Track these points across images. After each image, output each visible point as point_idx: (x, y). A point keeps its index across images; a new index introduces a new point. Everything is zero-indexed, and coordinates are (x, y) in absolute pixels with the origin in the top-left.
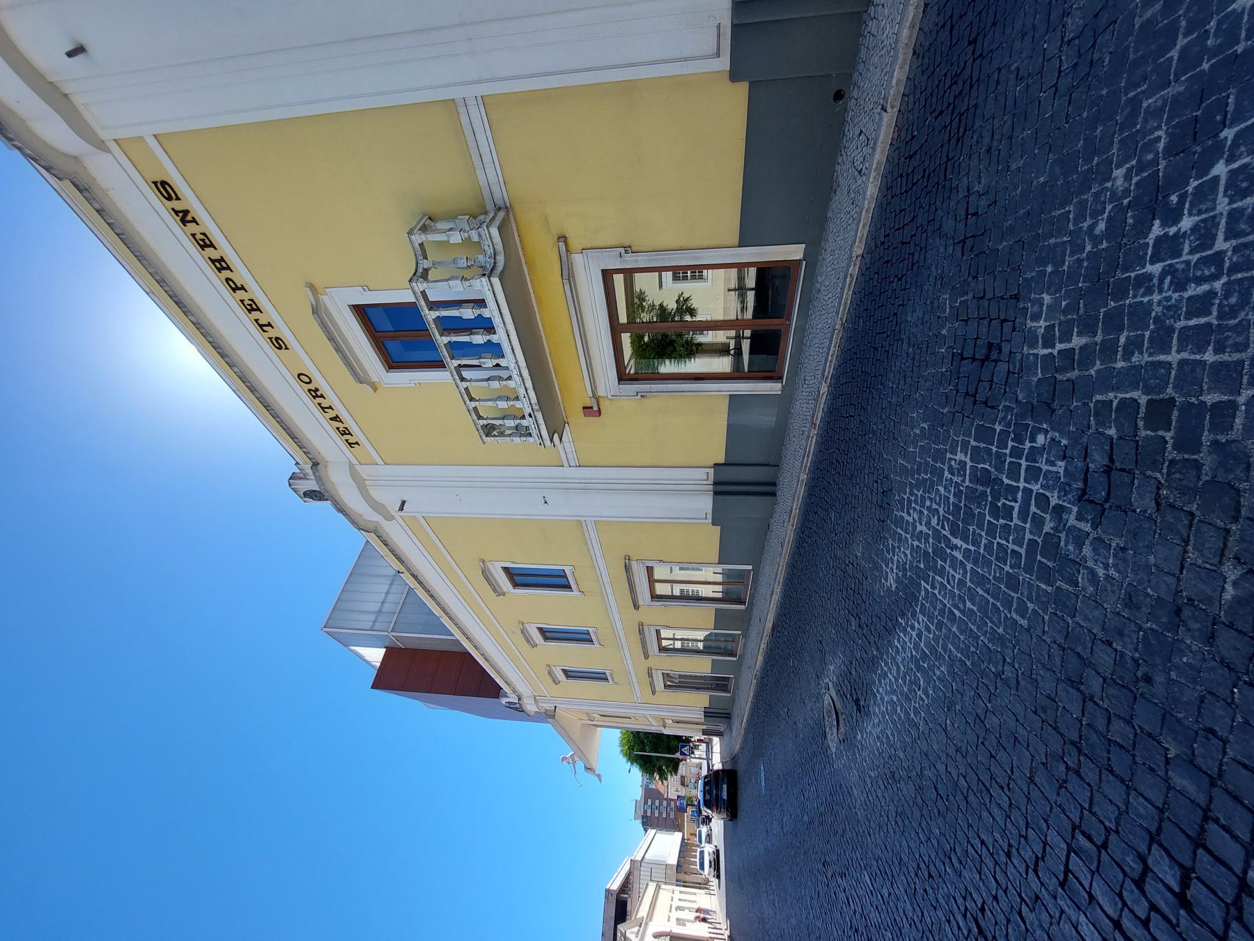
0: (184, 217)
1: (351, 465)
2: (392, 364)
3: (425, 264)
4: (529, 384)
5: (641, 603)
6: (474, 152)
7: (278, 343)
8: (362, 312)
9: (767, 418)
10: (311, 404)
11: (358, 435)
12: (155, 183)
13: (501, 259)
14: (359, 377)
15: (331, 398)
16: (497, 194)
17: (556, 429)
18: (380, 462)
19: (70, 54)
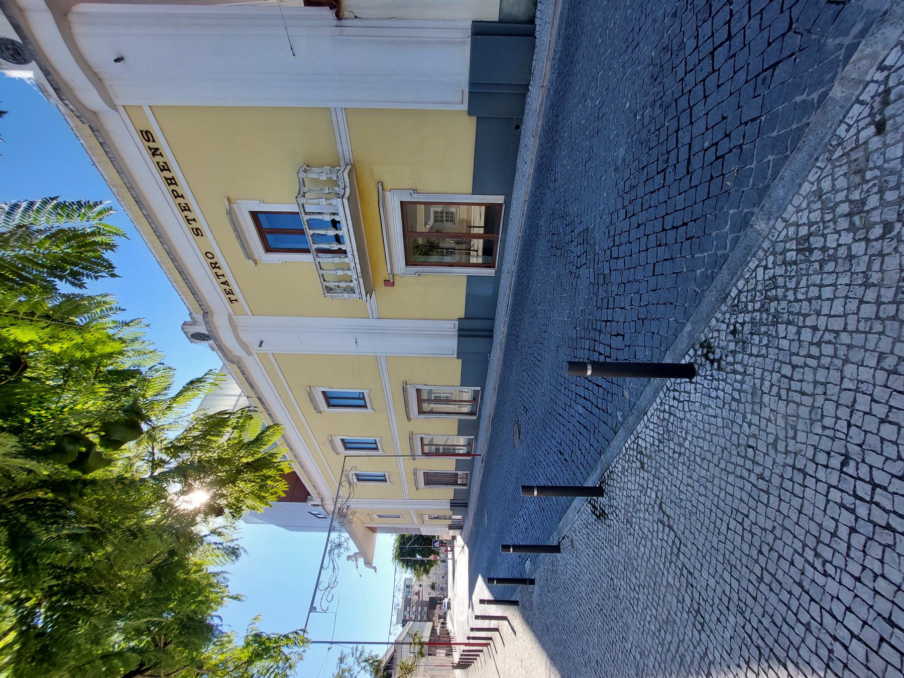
0: (155, 152)
1: (230, 315)
2: (268, 249)
3: (304, 189)
4: (357, 261)
5: (412, 417)
6: (337, 134)
7: (197, 232)
8: (255, 215)
9: (488, 291)
10: (210, 272)
11: (238, 294)
12: (141, 131)
13: (348, 190)
14: (249, 255)
15: (225, 269)
16: (347, 154)
17: (369, 291)
18: (249, 312)
19: (116, 61)
